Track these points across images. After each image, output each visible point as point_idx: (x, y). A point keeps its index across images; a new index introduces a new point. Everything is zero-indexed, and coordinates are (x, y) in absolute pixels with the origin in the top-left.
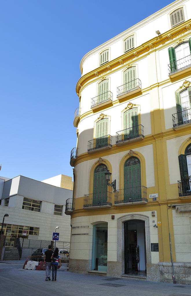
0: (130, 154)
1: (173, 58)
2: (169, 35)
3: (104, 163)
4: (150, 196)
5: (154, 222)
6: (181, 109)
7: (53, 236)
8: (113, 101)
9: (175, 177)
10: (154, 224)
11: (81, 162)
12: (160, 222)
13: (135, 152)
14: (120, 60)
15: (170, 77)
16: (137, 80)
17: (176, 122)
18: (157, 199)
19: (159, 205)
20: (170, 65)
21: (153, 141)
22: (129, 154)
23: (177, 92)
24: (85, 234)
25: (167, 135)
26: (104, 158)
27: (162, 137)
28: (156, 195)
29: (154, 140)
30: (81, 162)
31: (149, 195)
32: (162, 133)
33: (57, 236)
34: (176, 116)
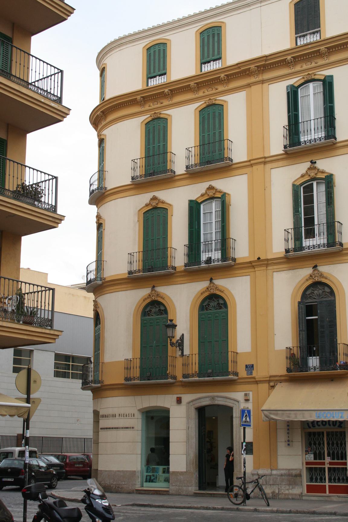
8: (108, 189)
14: (166, 90)
17: (291, 245)
19: (257, 382)
23: (295, 183)
27: (267, 265)
29: (253, 270)
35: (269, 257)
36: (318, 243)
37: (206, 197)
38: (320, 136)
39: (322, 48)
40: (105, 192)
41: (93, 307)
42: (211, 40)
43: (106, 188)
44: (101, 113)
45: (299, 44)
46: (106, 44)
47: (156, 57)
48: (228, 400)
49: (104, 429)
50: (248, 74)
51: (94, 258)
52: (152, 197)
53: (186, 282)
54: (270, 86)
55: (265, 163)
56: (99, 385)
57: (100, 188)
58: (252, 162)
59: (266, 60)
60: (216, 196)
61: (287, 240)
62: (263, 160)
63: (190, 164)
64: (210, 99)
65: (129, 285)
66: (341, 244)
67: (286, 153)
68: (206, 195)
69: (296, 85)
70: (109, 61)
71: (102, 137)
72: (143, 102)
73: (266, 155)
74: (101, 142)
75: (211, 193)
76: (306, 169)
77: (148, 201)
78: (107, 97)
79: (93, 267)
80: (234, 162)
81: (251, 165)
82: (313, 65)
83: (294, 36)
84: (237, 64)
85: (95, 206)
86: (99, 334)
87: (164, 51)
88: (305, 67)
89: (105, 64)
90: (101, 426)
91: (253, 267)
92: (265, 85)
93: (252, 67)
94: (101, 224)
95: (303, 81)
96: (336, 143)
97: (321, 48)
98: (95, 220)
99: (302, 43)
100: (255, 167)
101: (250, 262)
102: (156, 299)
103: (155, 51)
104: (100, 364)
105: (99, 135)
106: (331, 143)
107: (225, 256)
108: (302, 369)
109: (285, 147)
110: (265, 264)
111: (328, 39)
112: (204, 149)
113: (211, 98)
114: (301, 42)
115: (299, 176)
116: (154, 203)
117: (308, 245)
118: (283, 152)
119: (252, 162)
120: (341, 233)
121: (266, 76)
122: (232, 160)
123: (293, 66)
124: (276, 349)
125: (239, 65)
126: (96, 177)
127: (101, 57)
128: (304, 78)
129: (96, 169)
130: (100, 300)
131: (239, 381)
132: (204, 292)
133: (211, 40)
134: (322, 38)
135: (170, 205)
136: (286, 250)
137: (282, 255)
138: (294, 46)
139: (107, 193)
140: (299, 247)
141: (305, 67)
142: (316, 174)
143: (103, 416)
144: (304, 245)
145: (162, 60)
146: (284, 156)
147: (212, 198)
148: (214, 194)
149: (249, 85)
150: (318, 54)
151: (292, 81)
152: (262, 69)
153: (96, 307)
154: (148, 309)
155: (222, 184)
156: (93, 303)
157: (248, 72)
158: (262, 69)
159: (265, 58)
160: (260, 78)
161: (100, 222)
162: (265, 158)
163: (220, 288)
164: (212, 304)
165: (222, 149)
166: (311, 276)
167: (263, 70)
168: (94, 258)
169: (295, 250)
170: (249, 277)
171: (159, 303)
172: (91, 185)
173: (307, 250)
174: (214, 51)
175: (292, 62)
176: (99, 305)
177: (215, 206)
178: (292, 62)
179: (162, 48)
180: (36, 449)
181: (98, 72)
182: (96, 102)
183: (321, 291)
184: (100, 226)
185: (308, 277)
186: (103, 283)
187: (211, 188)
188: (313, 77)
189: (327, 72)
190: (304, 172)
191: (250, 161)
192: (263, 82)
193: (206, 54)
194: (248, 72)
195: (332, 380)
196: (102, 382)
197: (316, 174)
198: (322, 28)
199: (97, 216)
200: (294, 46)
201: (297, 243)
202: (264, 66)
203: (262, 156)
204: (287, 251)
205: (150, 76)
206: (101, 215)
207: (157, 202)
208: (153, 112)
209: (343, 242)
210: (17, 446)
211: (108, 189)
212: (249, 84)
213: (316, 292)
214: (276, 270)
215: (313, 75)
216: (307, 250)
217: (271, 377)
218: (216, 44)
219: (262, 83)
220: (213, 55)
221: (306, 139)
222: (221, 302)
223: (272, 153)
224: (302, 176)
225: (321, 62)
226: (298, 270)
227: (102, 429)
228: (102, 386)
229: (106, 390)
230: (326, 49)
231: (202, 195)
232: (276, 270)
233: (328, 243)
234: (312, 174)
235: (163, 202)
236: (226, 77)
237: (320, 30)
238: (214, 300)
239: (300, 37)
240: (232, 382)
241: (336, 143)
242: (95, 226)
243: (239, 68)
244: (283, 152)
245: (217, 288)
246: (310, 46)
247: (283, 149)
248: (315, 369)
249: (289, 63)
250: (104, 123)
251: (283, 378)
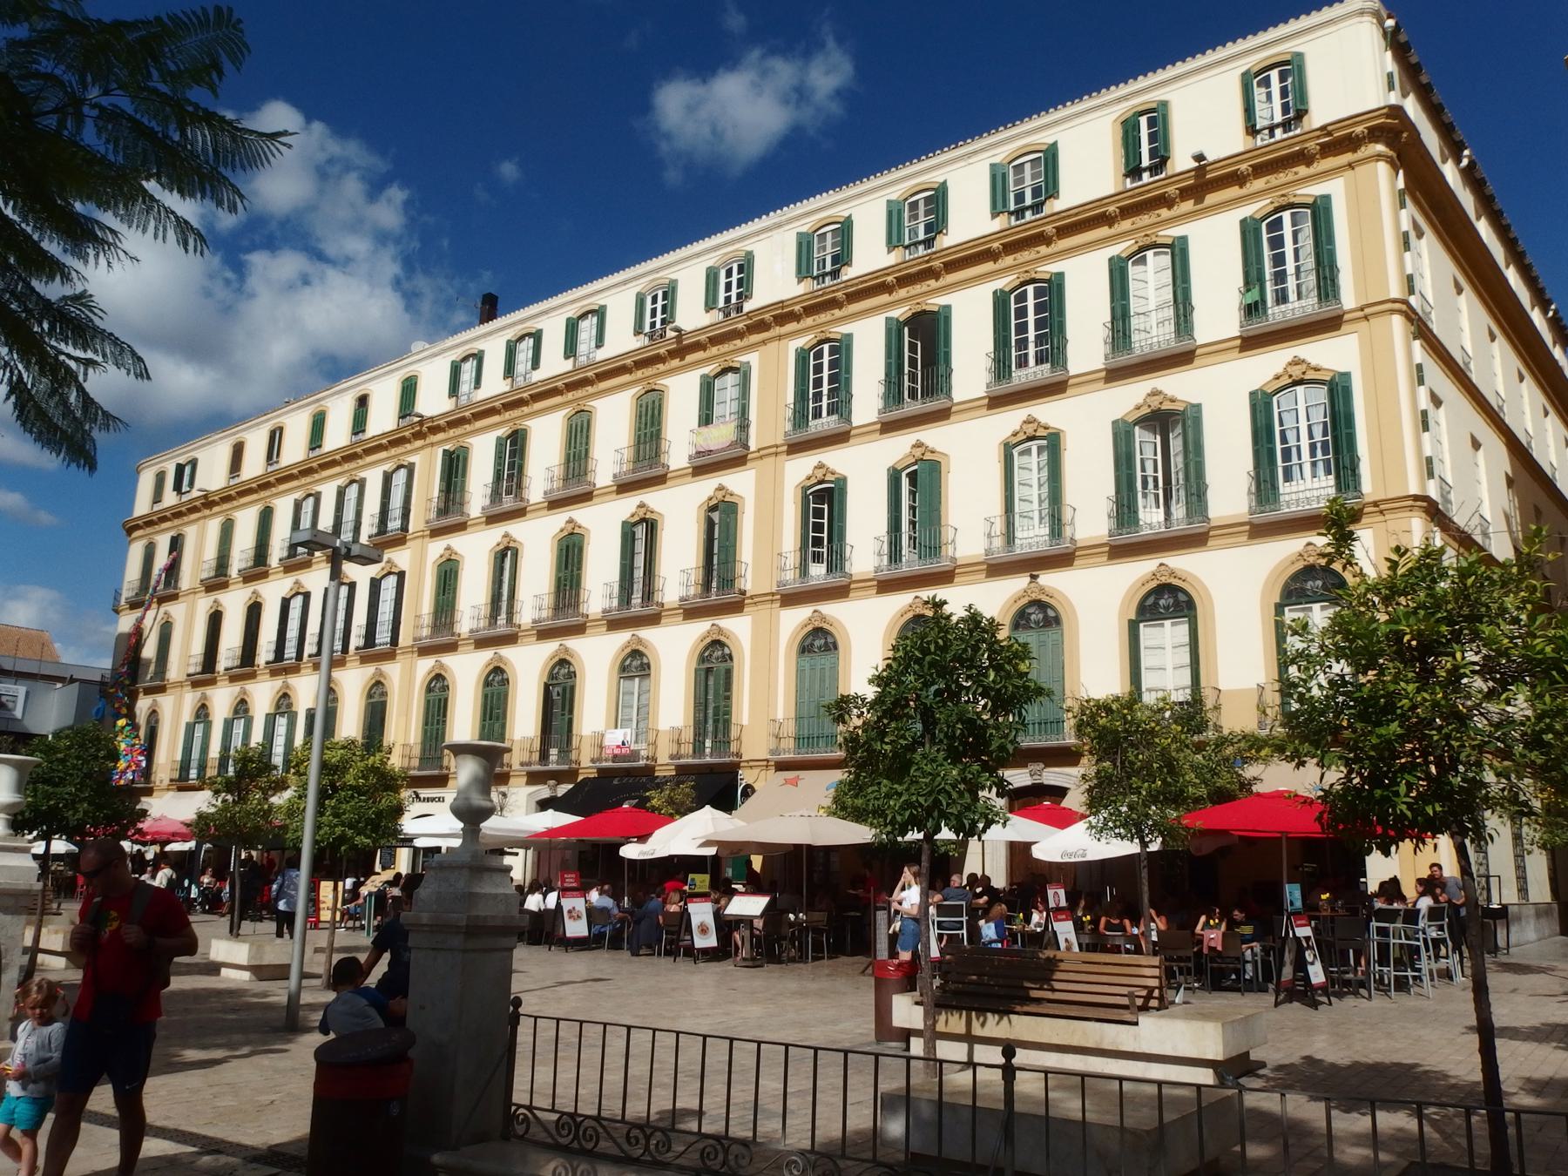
29: (1381, 518)
37: (1286, 381)
39: (839, 294)
58: (1368, 311)
60: (1306, 377)
75: (1030, 430)
77: (563, 525)
93: (767, 316)
112: (638, 451)
116: (918, 453)
119: (1368, 311)
149: (764, 342)
154: (1150, 601)
163: (1179, 574)
164: (817, 643)
187: (1030, 421)
189: (845, 329)
192: (780, 337)
213: (1162, 602)
225: (837, 313)
231: (1015, 435)
245: (1042, 590)
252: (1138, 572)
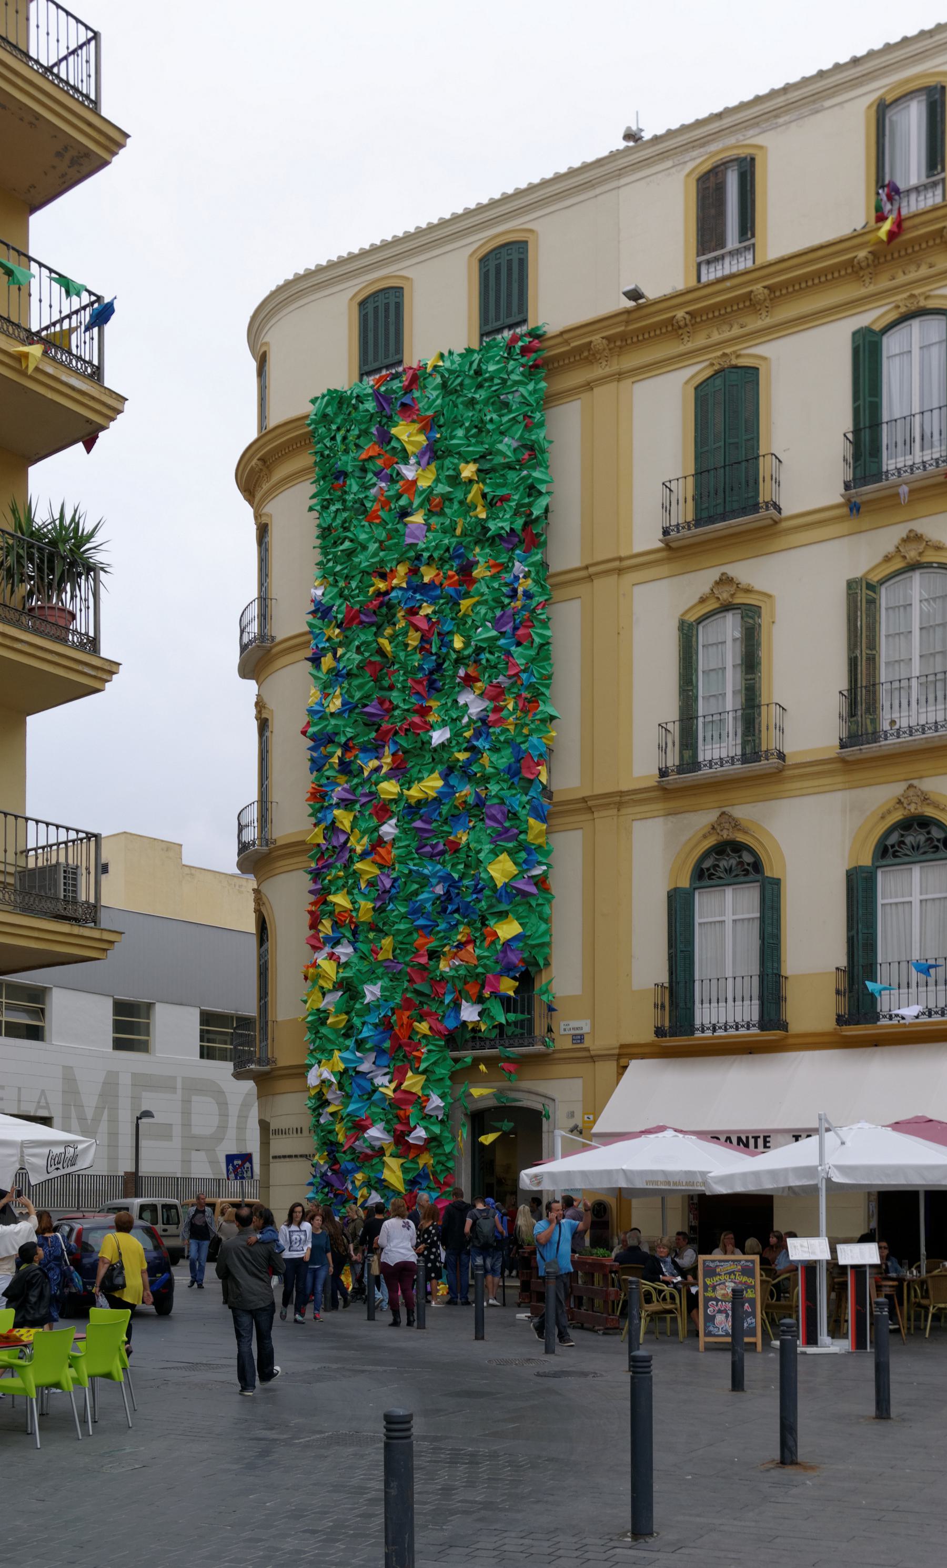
0: (905, 802)
1: (870, 396)
2: (862, 254)
3: (740, 837)
4: (562, 1027)
5: (572, 1115)
6: (697, 697)
7: (228, 1166)
8: (278, 639)
9: (649, 966)
10: (571, 1124)
11: (804, 792)
12: (591, 1117)
13: (932, 797)
14: (680, 314)
15: (667, 545)
16: (768, 457)
17: (673, 759)
18: (587, 1043)
19: (593, 1059)
20: (850, 436)
21: (583, 817)
22: (900, 802)
23: (686, 618)
24: (290, 1156)
25: (802, 777)
26: (741, 812)
27: (619, 806)
28: (585, 1026)
29: (589, 816)
30: (804, 792)
31: (562, 1024)
32: (621, 793)
33: (243, 1164)
34: (675, 729)
35: (624, 788)
36: (922, 722)
38: (936, 456)
40: (271, 648)
41: (252, 905)
42: (504, 276)
43: (273, 638)
44: (259, 463)
45: (704, 279)
46: (267, 293)
47: (725, 193)
48: (534, 1097)
49: (279, 1157)
50: (587, 358)
51: (255, 796)
52: (904, 535)
53: (840, 786)
54: (636, 386)
55: (620, 571)
56: (267, 1068)
57: (263, 636)
58: (592, 570)
59: (627, 323)
61: (663, 749)
62: (616, 564)
63: (674, 523)
64: (912, 296)
65: (839, 779)
66: (782, 756)
67: (668, 547)
68: (899, 559)
69: (877, 327)
70: (273, 337)
71: (264, 520)
72: (606, 353)
73: (623, 554)
74: (263, 531)
76: (710, 583)
78: (272, 422)
79: (253, 814)
80: (786, 512)
81: (590, 578)
82: (736, 331)
83: (693, 259)
84: (562, 334)
85: (254, 682)
86: (266, 962)
87: (399, 307)
88: (716, 337)
89: (266, 344)
90: (272, 1154)
91: (590, 810)
92: (626, 383)
94: (266, 720)
95: (893, 316)
96: (781, 520)
97: (593, 338)
98: (253, 712)
99: (712, 277)
100: (598, 583)
101: (584, 800)
102: (920, 810)
103: (510, 262)
104: (270, 1023)
105: (257, 516)
106: (770, 522)
107: (752, 751)
108: (511, 1042)
109: (847, 486)
110: (615, 803)
111: (771, 265)
113: (916, 292)
114: (709, 274)
115: (696, 599)
117: (708, 758)
118: (661, 545)
120: (782, 730)
121: (629, 361)
122: (779, 510)
123: (873, 276)
124: (634, 988)
125: (566, 336)
126: (254, 611)
127: (259, 320)
128: (712, 364)
129: (254, 593)
130: (266, 889)
131: (557, 1056)
132: (889, 812)
133: (504, 276)
134: (759, 262)
135: (769, 596)
136: (660, 770)
137: (652, 782)
138: (693, 283)
139: (275, 650)
140: (689, 763)
141: (716, 337)
142: (732, 595)
143: (276, 1132)
144: (700, 759)
145: (515, 286)
146: (664, 554)
147: (727, 608)
148: (920, 554)
150: (749, 304)
151: (867, 318)
152: (618, 343)
153: (259, 905)
155: (758, 573)
156: (253, 896)
157: (586, 354)
158: (618, 343)
159: (624, 317)
160: (615, 366)
161: (264, 716)
162: (621, 559)
165: (753, 482)
166: (713, 828)
167: (620, 347)
168: (253, 794)
169: (681, 770)
170: (579, 832)
171: (737, 847)
172: (242, 632)
173: (892, 740)
174: (509, 304)
175: (686, 325)
176: (264, 899)
177: (729, 628)
178: (686, 325)
179: (392, 301)
180: (175, 1201)
181: (253, 365)
182: (252, 434)
183: (733, 862)
184: (263, 725)
185: (706, 830)
186: (271, 852)
187: (913, 538)
188: (922, 303)
190: (890, 548)
191: (587, 568)
192: (620, 376)
193: (371, 357)
194: (586, 354)
195: (876, 1046)
196: (274, 1062)
197: (732, 595)
198: (758, 240)
199: (257, 704)
200: (693, 283)
201: (687, 754)
202: (623, 337)
203: (615, 555)
204: (663, 773)
205: (367, 369)
206: (266, 700)
207: (733, 590)
208: (719, 353)
209: (786, 751)
210: (136, 1196)
211: (278, 639)
212: (588, 384)
214: (639, 816)
215: (733, 357)
216: (892, 740)
217: (622, 1046)
218: (515, 286)
219: (619, 380)
220: (509, 314)
221: (899, 465)
222: (747, 858)
223: (637, 549)
224: (703, 600)
225: (755, 323)
226: (687, 815)
227: (275, 1157)
228: (272, 1070)
229: (282, 1077)
230: (766, 291)
232: (639, 816)
233: (743, 755)
234: (725, 596)
235: (748, 591)
236: (688, 317)
237: (754, 245)
238: (728, 855)
239: (708, 262)
240: (542, 1059)
241: (781, 520)
242: (253, 726)
243: (567, 342)
244: (661, 545)
246: (728, 284)
247: (661, 536)
248: (714, 1030)
249: (680, 328)
250: (266, 487)
251: (647, 1050)
252: (698, 824)
